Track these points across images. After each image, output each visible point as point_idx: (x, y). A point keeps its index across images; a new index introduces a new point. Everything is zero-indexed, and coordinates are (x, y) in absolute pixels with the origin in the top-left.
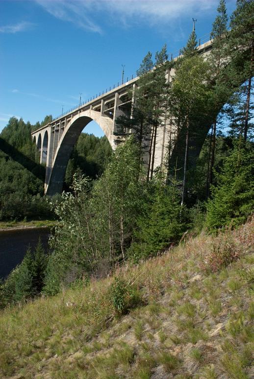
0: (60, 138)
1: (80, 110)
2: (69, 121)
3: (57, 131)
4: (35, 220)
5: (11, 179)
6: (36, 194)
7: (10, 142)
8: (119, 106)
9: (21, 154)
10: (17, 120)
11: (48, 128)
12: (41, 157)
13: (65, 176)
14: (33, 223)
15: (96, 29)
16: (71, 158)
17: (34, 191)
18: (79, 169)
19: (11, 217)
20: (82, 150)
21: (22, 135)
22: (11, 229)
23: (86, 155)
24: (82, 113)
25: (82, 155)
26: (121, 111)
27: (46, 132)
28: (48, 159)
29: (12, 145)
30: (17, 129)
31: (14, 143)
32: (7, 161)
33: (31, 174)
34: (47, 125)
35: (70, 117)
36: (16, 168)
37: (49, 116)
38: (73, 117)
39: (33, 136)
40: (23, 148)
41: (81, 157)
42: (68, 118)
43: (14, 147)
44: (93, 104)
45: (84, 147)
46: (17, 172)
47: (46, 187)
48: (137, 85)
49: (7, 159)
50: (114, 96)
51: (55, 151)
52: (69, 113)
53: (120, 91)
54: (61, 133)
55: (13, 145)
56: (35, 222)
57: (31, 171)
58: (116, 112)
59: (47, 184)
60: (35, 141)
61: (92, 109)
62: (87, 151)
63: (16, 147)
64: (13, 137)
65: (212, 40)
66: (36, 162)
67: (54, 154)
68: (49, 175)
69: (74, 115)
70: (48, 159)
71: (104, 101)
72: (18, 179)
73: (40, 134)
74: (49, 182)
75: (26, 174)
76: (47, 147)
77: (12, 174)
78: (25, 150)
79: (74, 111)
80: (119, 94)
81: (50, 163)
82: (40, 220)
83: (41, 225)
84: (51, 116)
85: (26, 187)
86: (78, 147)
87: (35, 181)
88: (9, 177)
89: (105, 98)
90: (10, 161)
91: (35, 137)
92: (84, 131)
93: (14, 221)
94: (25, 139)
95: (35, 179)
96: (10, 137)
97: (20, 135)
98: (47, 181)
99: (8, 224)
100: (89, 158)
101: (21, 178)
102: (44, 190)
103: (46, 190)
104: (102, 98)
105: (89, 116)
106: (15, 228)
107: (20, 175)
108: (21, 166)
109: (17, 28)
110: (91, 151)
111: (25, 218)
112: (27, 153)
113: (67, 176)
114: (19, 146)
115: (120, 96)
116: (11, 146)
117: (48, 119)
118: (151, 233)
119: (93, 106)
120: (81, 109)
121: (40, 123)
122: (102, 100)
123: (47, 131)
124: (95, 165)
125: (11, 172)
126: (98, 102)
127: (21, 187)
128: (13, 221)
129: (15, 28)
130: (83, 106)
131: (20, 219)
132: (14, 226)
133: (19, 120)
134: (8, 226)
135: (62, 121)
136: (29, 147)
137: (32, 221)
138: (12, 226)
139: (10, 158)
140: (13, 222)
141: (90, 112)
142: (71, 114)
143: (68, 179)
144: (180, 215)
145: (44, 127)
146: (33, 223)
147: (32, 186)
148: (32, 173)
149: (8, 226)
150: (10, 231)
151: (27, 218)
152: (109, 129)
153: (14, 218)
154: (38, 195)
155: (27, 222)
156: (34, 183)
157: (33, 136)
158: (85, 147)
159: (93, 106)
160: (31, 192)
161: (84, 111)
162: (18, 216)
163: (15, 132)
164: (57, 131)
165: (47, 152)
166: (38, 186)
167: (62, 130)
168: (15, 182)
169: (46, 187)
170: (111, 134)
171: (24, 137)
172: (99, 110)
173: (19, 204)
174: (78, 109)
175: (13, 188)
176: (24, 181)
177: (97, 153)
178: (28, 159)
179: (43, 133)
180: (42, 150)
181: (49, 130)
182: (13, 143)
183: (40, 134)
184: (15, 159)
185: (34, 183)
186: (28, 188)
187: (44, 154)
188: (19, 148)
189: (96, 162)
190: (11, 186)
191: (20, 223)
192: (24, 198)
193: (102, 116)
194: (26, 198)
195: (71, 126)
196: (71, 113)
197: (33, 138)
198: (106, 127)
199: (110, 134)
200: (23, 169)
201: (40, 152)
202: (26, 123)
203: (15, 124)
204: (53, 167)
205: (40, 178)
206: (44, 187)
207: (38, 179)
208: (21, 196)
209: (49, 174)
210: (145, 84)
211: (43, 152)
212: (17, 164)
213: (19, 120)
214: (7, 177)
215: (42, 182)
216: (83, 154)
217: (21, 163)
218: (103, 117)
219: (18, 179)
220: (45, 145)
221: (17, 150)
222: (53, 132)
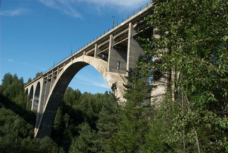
1: (73, 58)
3: (50, 80)
6: (26, 137)
7: (4, 93)
8: (114, 46)
10: (12, 76)
11: (41, 79)
12: (32, 105)
13: (54, 121)
15: (77, 15)
16: (60, 106)
17: (25, 135)
18: (67, 115)
20: (68, 100)
21: (16, 88)
23: (72, 104)
25: (69, 104)
26: (115, 51)
27: (39, 83)
28: (39, 106)
30: (11, 83)
31: (8, 95)
33: (23, 120)
34: (39, 77)
36: (9, 114)
38: (65, 65)
41: (68, 106)
43: (7, 97)
46: (9, 118)
47: (36, 131)
48: (133, 24)
50: (109, 38)
52: (62, 62)
53: (114, 33)
54: (53, 84)
55: (5, 98)
58: (111, 51)
62: (72, 102)
63: (9, 97)
64: (7, 89)
65: (123, 100)
66: (27, 110)
69: (66, 64)
70: (39, 106)
73: (32, 86)
74: (39, 126)
75: (17, 120)
77: (4, 119)
78: (18, 100)
79: (67, 59)
80: (114, 36)
81: (41, 109)
85: (17, 131)
86: (65, 98)
92: (71, 85)
95: (26, 124)
97: (14, 87)
100: (75, 107)
101: (13, 123)
102: (34, 134)
103: (36, 134)
105: (82, 61)
107: (12, 121)
108: (13, 113)
109: (16, 13)
110: (76, 101)
112: (19, 102)
113: (56, 121)
114: (12, 97)
115: (114, 38)
117: (38, 75)
120: (74, 56)
121: (32, 79)
122: (96, 45)
124: (80, 112)
127: (12, 130)
129: (14, 12)
133: (13, 76)
135: (54, 71)
141: (83, 57)
147: (23, 130)
148: (23, 119)
152: (103, 67)
154: (28, 138)
157: (26, 88)
158: (71, 99)
159: (86, 52)
160: (21, 135)
161: (76, 57)
164: (50, 80)
165: (38, 101)
166: (29, 130)
167: (54, 79)
170: (107, 71)
172: (93, 55)
174: (71, 57)
177: (82, 102)
179: (35, 85)
181: (41, 81)
182: (7, 95)
183: (32, 86)
184: (7, 107)
186: (19, 132)
187: (35, 102)
188: (12, 98)
189: (82, 110)
194: (16, 140)
195: (67, 69)
196: (64, 62)
197: (25, 91)
198: (100, 66)
199: (105, 71)
201: (32, 102)
202: (19, 78)
203: (9, 79)
207: (28, 124)
208: (11, 138)
209: (39, 119)
211: (35, 100)
212: (8, 111)
213: (13, 76)
215: (32, 127)
217: (14, 111)
219: (10, 124)
220: (37, 94)
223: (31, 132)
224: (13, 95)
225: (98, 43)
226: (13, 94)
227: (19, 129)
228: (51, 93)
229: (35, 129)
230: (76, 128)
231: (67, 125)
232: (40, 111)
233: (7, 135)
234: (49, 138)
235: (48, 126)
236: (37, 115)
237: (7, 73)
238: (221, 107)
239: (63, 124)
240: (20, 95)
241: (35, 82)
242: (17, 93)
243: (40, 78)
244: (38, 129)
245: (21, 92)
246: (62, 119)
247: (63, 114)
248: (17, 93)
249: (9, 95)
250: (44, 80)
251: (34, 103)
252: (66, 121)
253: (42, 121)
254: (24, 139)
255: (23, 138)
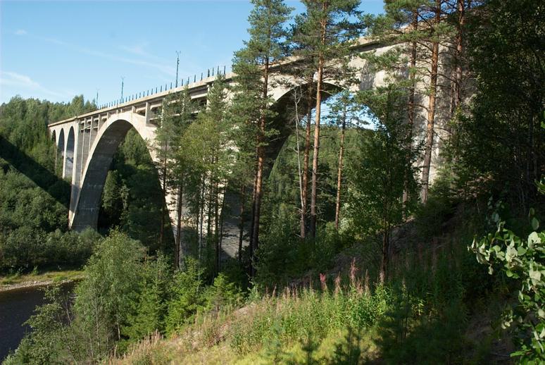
0: (92, 144)
1: (119, 109)
2: (105, 120)
3: (88, 131)
4: (51, 271)
5: (12, 205)
6: (53, 229)
7: (12, 139)
9: (31, 161)
14: (49, 276)
16: (112, 168)
19: (10, 268)
21: (33, 128)
22: (11, 288)
24: (121, 114)
28: (75, 171)
29: (16, 145)
30: (23, 117)
31: (19, 141)
32: (5, 172)
33: (48, 196)
35: (106, 115)
36: (22, 185)
37: (79, 96)
38: (109, 116)
39: (52, 129)
40: (34, 149)
41: (129, 166)
42: (104, 115)
44: (137, 105)
45: (134, 149)
46: (23, 193)
47: (72, 216)
49: (6, 169)
51: (84, 162)
54: (94, 136)
56: (52, 274)
57: (46, 189)
59: (73, 211)
60: (54, 138)
61: (134, 112)
63: (22, 149)
67: (84, 166)
68: (75, 198)
70: (75, 171)
71: (150, 104)
72: (25, 205)
73: (62, 130)
75: (38, 196)
76: (73, 151)
78: (37, 152)
81: (78, 179)
82: (59, 271)
83: (62, 279)
84: (82, 96)
85: (38, 217)
87: (53, 207)
88: (10, 202)
89: (151, 102)
90: (11, 174)
91: (54, 131)
93: (17, 275)
94: (38, 135)
95: (54, 203)
96: (10, 130)
98: (73, 206)
99: (5, 279)
102: (68, 221)
104: (148, 101)
106: (17, 286)
107: (28, 199)
108: (31, 181)
111: (35, 268)
112: (41, 160)
114: (27, 145)
116: (13, 146)
118: (145, 316)
119: (136, 107)
120: (120, 108)
123: (72, 127)
125: (13, 193)
126: (142, 104)
128: (14, 274)
130: (123, 105)
131: (27, 271)
132: (16, 283)
134: (5, 283)
136: (44, 149)
137: (48, 273)
138: (11, 283)
139: (11, 167)
140: (13, 277)
142: (108, 111)
143: (107, 202)
144: (491, 199)
145: (69, 120)
146: (49, 276)
147: (47, 215)
149: (5, 283)
150: (9, 291)
151: (38, 269)
153: (16, 270)
155: (38, 274)
156: (52, 210)
159: (136, 107)
160: (47, 227)
162: (24, 267)
163: (21, 122)
164: (88, 131)
165: (73, 159)
166: (59, 215)
167: (95, 132)
168: (19, 209)
169: (72, 216)
171: (35, 132)
173: (24, 247)
175: (16, 220)
176: (34, 208)
178: (42, 169)
180: (65, 154)
183: (62, 130)
184: (20, 169)
185: (52, 210)
186: (42, 219)
190: (12, 218)
191: (26, 277)
192: (33, 237)
193: (147, 126)
200: (33, 187)
204: (81, 186)
205: (62, 203)
206: (68, 217)
207: (58, 203)
209: (76, 196)
210: (137, 164)
211: (68, 158)
212: (24, 178)
214: (6, 203)
215: (65, 208)
216: (133, 160)
217: (31, 176)
218: (148, 128)
219: (25, 205)
220: (71, 148)
221: (24, 153)
222: (82, 131)
223: (62, 218)
224: (29, 142)
226: (28, 139)
227: (41, 214)
228: (90, 158)
229: (70, 212)
230: (434, 175)
231: (125, 205)
232: (76, 183)
233: (21, 229)
234: (93, 230)
235: (92, 209)
236: (72, 187)
237: (14, 96)
238: (517, 160)
239: (118, 203)
240: (42, 144)
241: (66, 124)
242: (36, 137)
243: (73, 121)
244: (74, 214)
245: (43, 137)
246: (116, 192)
247: (119, 183)
248: (36, 137)
249: (21, 142)
250: (80, 129)
251: (66, 163)
252: (124, 198)
253: (79, 202)
254: (51, 234)
255: (48, 232)
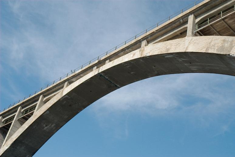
225: (196, 14)
